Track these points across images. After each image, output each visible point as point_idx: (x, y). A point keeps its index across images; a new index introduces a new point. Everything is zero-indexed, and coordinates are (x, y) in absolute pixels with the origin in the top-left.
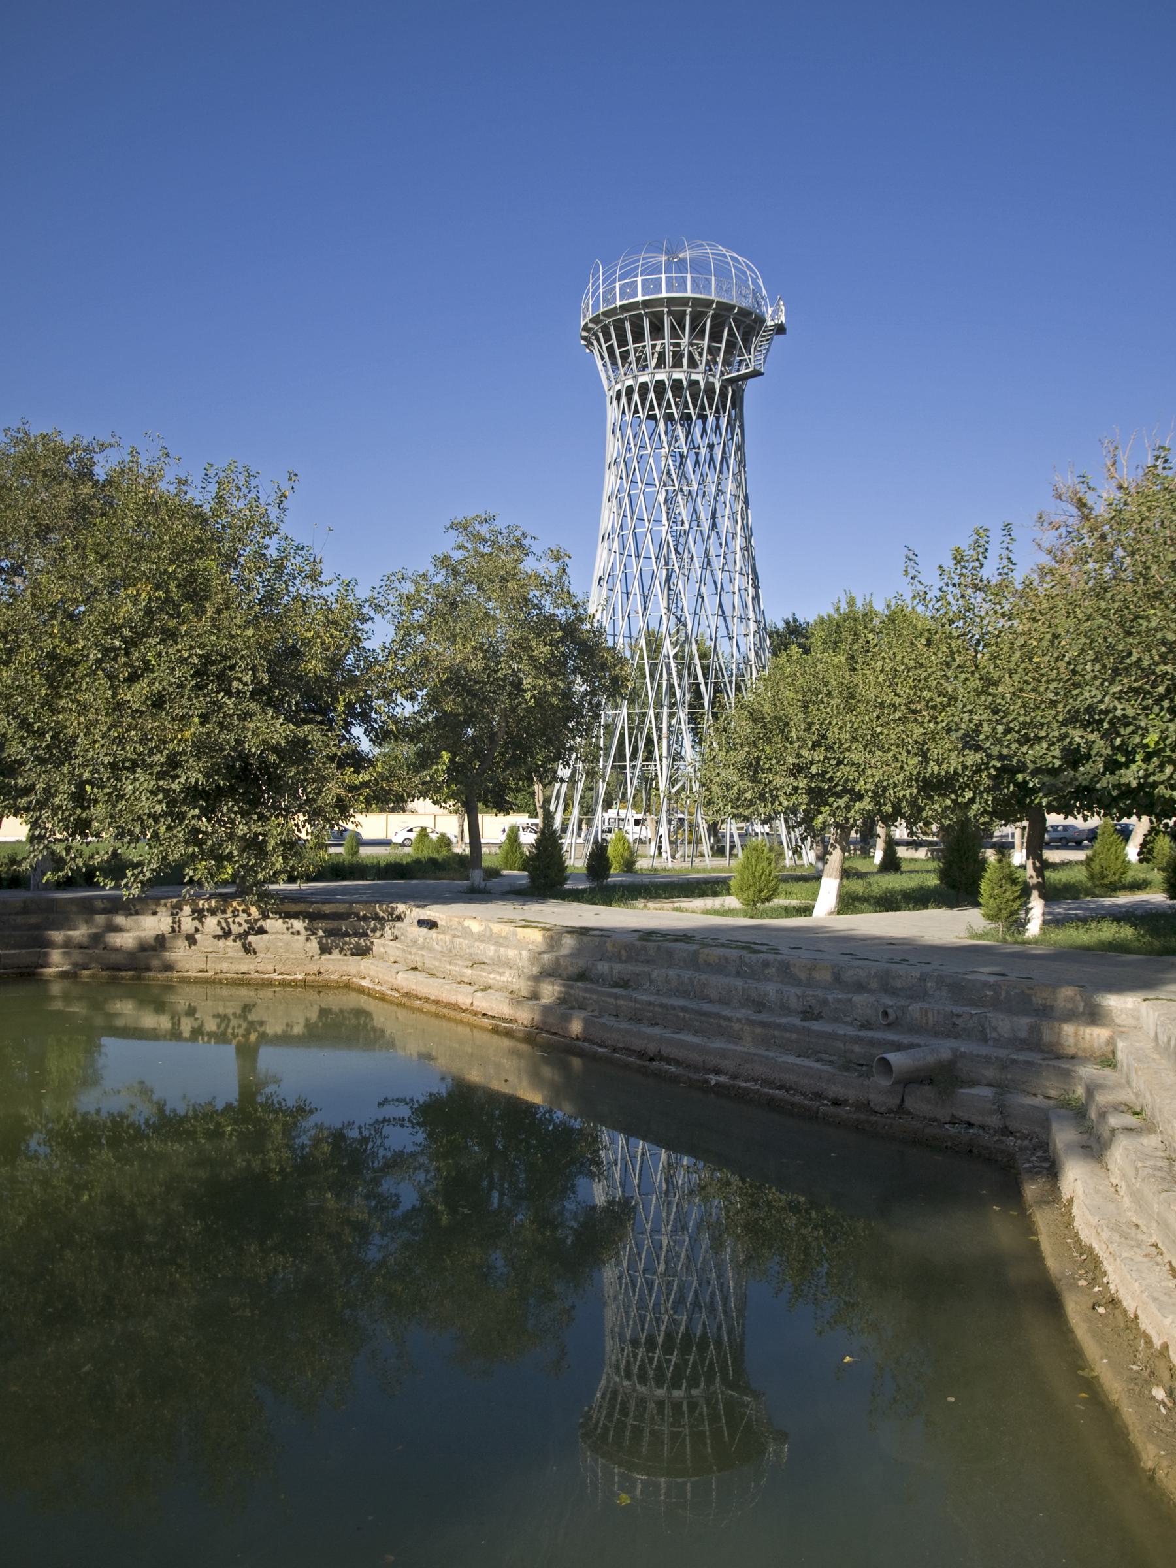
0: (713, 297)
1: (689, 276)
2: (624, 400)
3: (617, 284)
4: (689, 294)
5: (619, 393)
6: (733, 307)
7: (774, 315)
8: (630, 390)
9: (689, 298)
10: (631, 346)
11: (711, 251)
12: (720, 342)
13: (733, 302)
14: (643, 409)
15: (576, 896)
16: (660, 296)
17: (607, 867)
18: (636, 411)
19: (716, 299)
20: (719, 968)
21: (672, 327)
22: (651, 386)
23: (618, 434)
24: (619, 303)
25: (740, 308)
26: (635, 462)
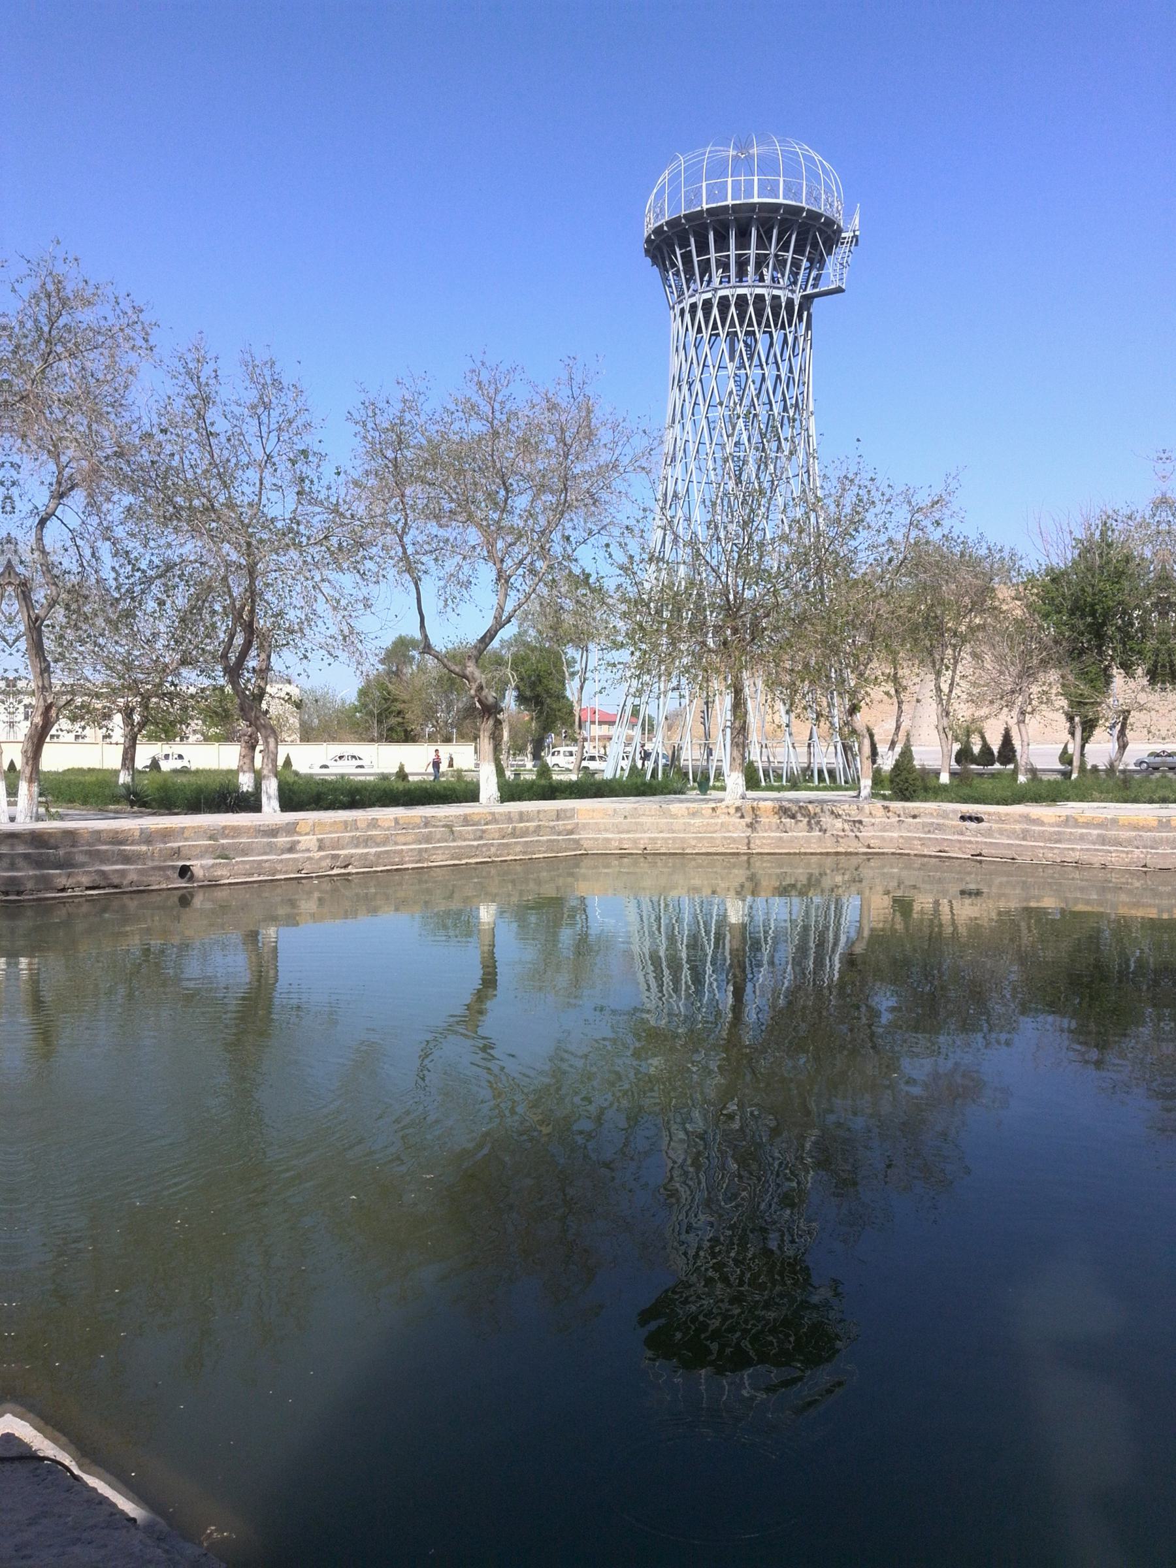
0: (804, 205)
1: (781, 180)
2: (687, 316)
3: (704, 184)
4: (781, 200)
5: (693, 307)
6: (821, 215)
7: (851, 226)
8: (707, 304)
9: (779, 206)
10: (713, 255)
11: (801, 149)
12: (788, 251)
13: (822, 211)
14: (723, 326)
15: (764, 789)
16: (751, 201)
17: (708, 779)
18: (715, 327)
19: (807, 207)
20: (1087, 825)
21: (759, 236)
22: (715, 302)
23: (682, 353)
24: (705, 207)
25: (826, 218)
26: (714, 383)
